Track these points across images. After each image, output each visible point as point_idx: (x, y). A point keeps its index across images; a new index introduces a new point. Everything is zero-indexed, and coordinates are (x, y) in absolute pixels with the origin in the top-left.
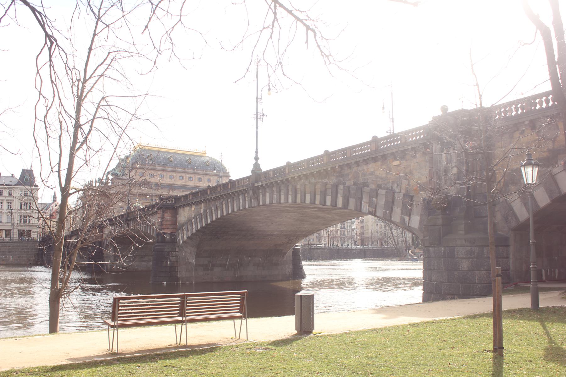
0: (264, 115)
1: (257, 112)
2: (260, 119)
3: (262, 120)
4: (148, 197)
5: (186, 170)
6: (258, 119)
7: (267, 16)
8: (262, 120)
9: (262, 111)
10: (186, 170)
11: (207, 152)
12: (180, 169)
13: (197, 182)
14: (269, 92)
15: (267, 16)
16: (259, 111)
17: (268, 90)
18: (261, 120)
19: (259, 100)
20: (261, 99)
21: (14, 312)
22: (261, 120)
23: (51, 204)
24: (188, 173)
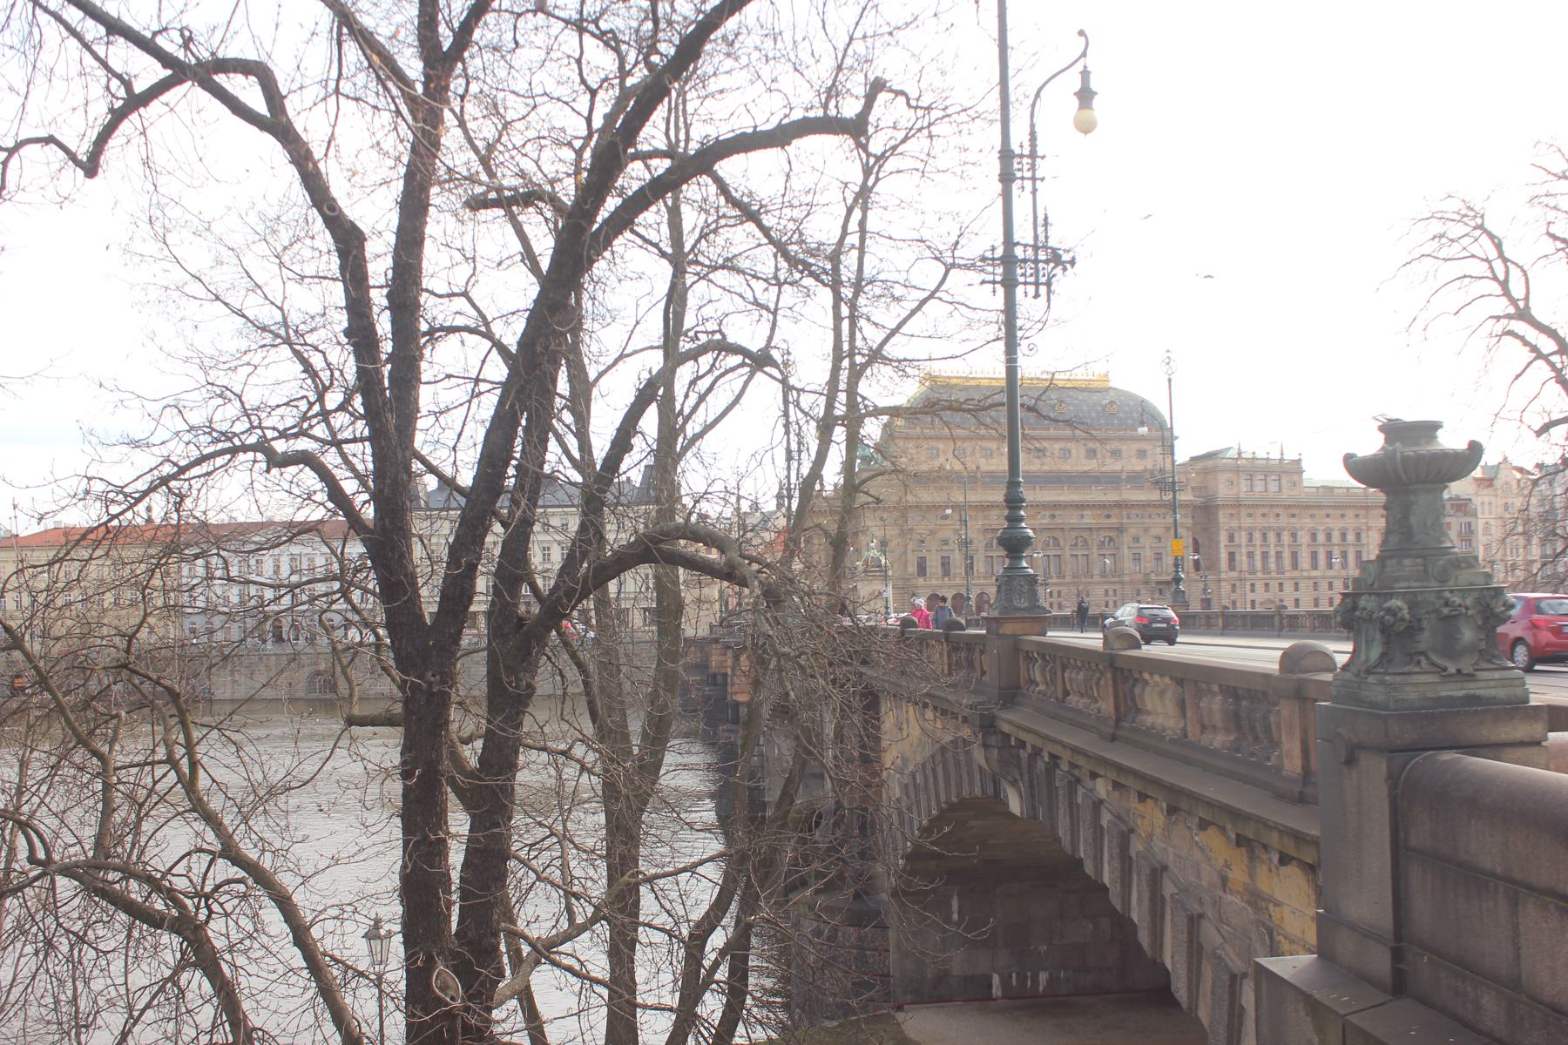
0: (1055, 258)
1: (1009, 242)
2: (1031, 289)
3: (1043, 289)
4: (949, 511)
5: (1052, 431)
6: (1020, 290)
7: (1517, 377)
8: (1043, 289)
9: (1040, 230)
10: (1052, 431)
11: (1110, 377)
12: (1034, 429)
13: (1084, 461)
14: (1086, 112)
15: (1517, 377)
16: (1023, 233)
17: (1075, 102)
18: (1037, 296)
19: (1021, 167)
20: (1033, 155)
21: (1154, 496)
22: (1037, 296)
23: (775, 512)
24: (1057, 439)
